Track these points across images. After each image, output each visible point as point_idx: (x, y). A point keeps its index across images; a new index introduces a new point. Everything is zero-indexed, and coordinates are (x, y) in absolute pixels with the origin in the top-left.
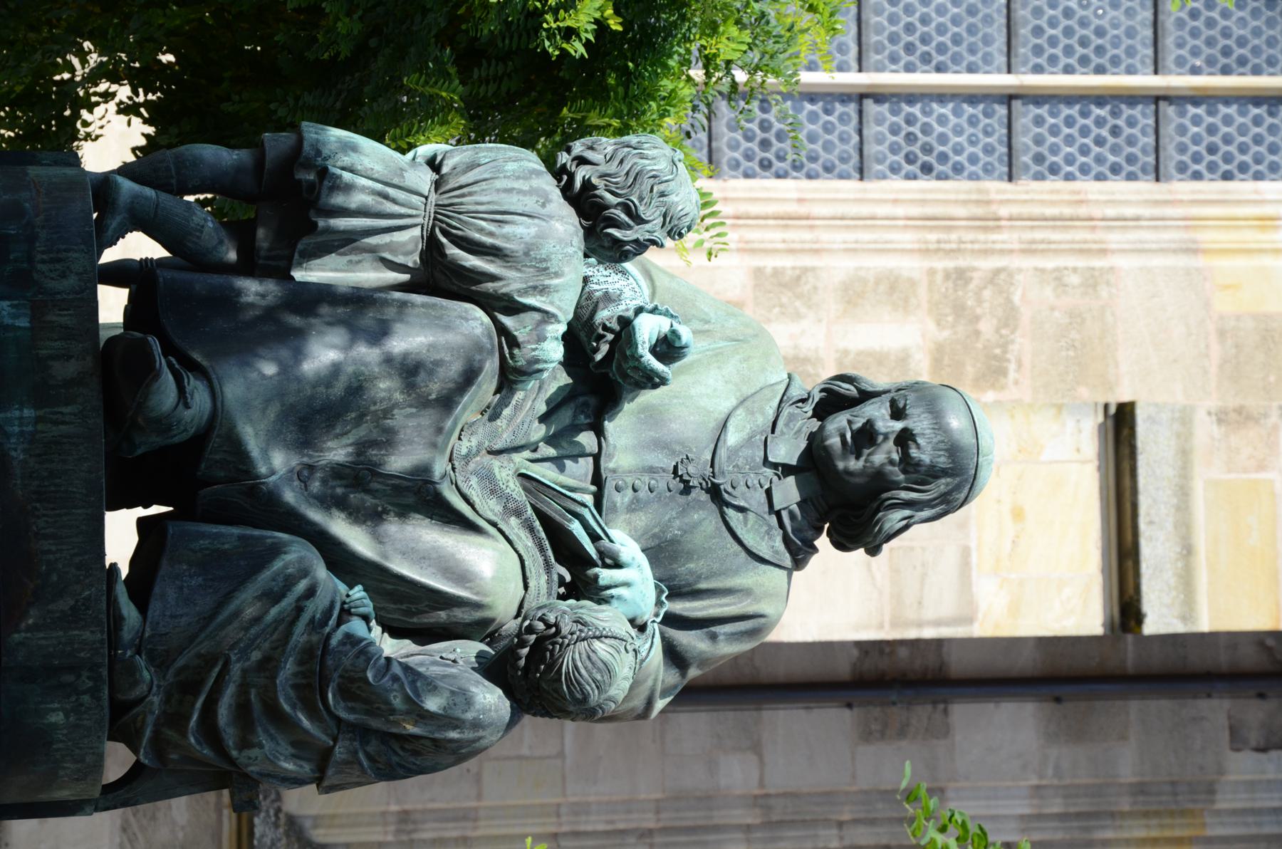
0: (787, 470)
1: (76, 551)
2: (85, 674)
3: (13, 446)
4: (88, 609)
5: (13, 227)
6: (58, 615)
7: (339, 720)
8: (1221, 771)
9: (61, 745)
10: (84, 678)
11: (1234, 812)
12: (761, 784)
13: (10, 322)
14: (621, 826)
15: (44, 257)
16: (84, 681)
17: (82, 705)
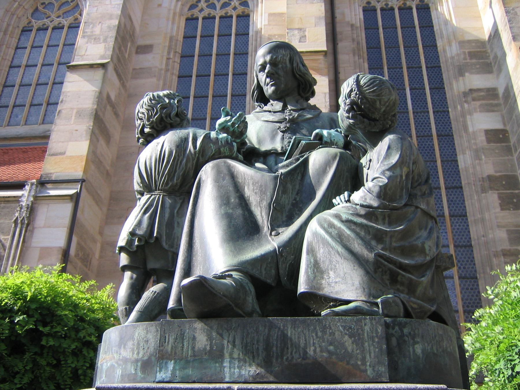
0: (284, 107)
1: (314, 335)
2: (391, 331)
3: (247, 373)
4: (350, 328)
5: (118, 372)
6: (355, 346)
7: (406, 205)
9: (434, 348)
10: (394, 332)
13: (170, 372)
15: (136, 353)
16: (395, 332)
17: (410, 333)
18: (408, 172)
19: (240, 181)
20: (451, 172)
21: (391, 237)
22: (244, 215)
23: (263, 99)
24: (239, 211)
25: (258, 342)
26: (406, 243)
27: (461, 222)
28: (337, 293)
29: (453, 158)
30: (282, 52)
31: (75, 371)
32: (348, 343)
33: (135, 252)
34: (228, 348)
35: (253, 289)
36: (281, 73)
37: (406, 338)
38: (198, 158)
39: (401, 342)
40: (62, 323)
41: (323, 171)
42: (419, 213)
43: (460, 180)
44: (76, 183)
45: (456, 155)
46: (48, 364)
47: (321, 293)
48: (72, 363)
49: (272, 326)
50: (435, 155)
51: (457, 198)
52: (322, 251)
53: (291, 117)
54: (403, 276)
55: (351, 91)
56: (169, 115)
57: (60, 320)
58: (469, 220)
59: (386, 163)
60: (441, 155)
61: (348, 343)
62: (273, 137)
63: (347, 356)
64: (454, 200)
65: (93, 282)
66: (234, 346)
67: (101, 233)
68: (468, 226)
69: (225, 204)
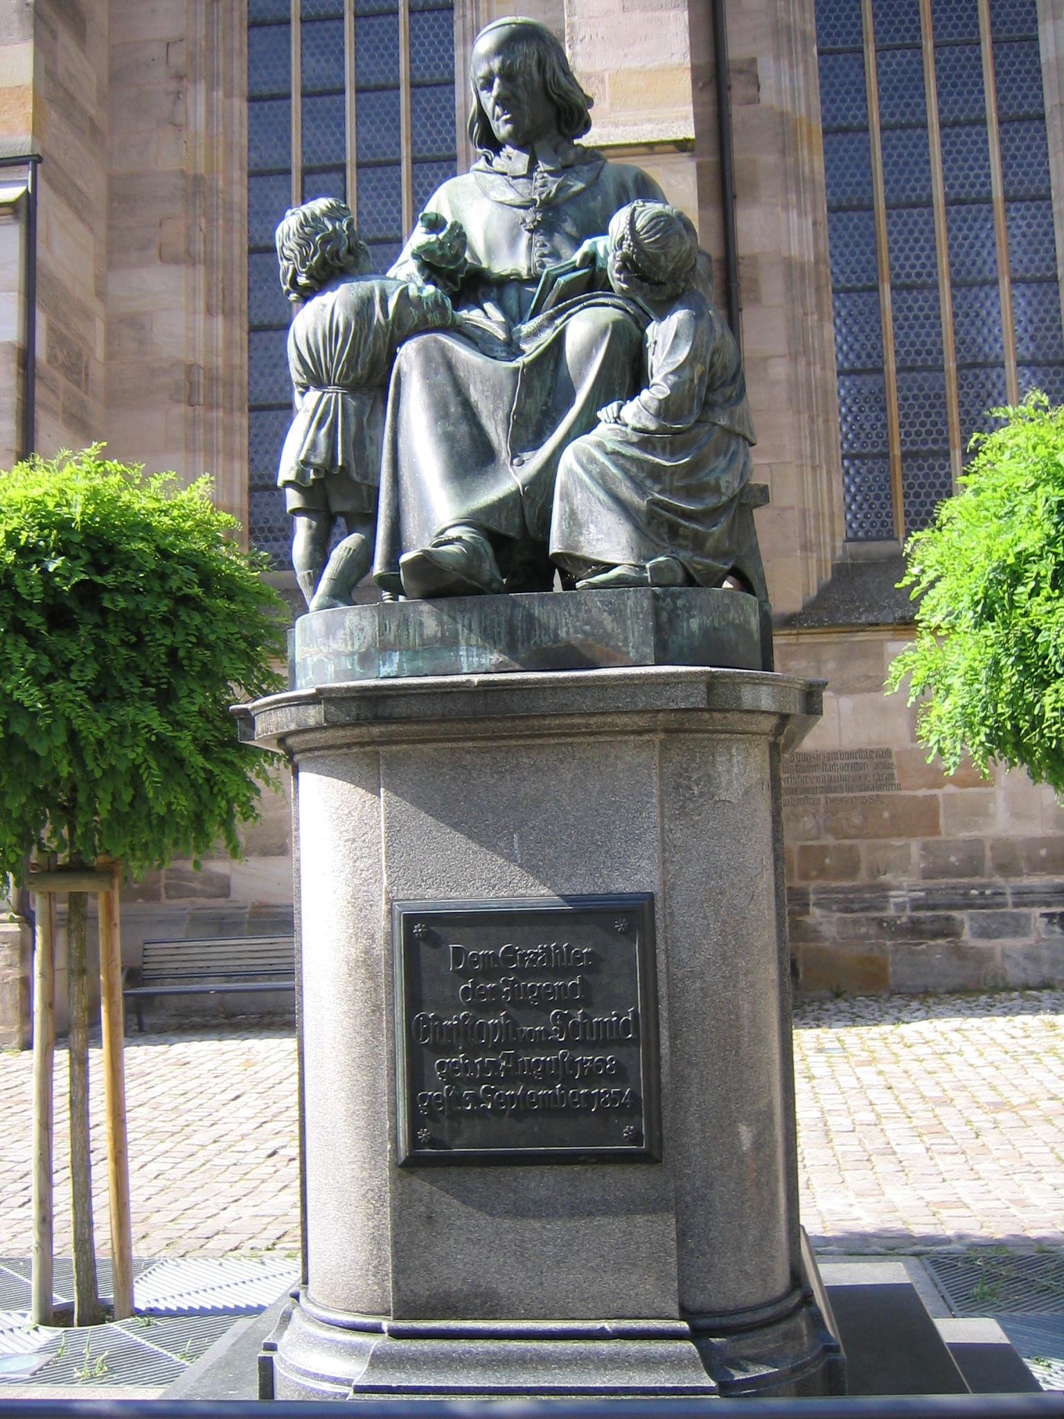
0: (532, 166)
2: (661, 604)
7: (698, 422)
8: (771, 108)
11: (793, 102)
12: (784, 356)
14: (807, 432)
18: (703, 372)
19: (462, 374)
20: (1018, 72)
21: (672, 474)
22: (471, 434)
23: (491, 143)
24: (464, 428)
25: (499, 624)
26: (693, 481)
27: (1034, 217)
28: (599, 553)
29: (1025, 33)
30: (523, 48)
31: (172, 652)
32: (608, 622)
33: (310, 488)
34: (463, 634)
35: (490, 550)
36: (522, 94)
37: (680, 612)
38: (392, 331)
39: (673, 617)
40: (133, 565)
41: (587, 356)
42: (717, 432)
43: (1039, 98)
44: (17, 168)
45: (1035, 21)
46: (124, 643)
47: (578, 554)
48: (164, 637)
49: (515, 604)
50: (977, 26)
51: (1028, 148)
52: (579, 496)
53: (544, 196)
54: (685, 527)
55: (623, 238)
56: (335, 255)
57: (128, 561)
58: (1055, 208)
59: (670, 361)
60: (993, 24)
61: (608, 622)
62: (513, 242)
63: (606, 637)
64: (1019, 154)
65: (170, 475)
66: (470, 630)
67: (101, 294)
68: (1051, 224)
69: (442, 417)
